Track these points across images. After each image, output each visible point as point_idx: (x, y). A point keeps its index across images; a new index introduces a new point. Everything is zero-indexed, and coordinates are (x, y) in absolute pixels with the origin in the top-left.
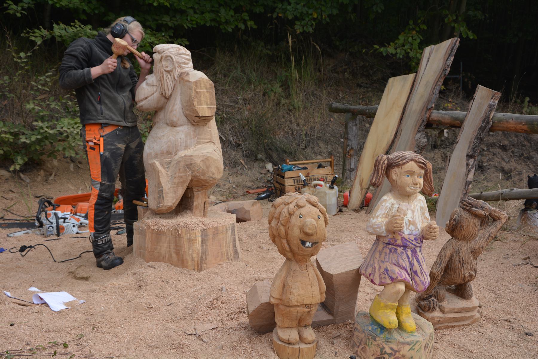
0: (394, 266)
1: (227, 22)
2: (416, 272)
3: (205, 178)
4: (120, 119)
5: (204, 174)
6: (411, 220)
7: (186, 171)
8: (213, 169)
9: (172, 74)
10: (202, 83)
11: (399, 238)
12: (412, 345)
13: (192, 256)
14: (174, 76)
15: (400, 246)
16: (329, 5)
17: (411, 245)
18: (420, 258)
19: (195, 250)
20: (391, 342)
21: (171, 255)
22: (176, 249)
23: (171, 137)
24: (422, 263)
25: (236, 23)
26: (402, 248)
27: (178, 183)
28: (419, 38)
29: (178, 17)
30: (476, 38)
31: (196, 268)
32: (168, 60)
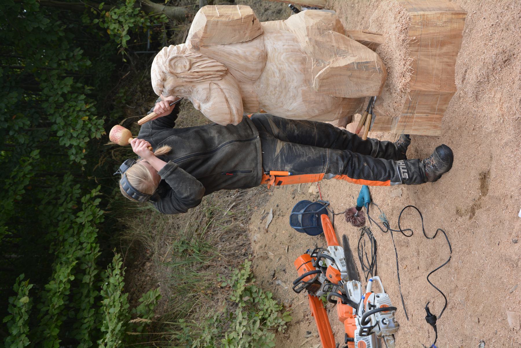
1: (94, 214)
4: (252, 147)
9: (194, 61)
13: (445, 22)
14: (197, 57)
16: (75, 104)
19: (438, 18)
21: (446, 54)
22: (437, 46)
23: (282, 57)
28: (113, 10)
29: (84, 266)
31: (461, 16)
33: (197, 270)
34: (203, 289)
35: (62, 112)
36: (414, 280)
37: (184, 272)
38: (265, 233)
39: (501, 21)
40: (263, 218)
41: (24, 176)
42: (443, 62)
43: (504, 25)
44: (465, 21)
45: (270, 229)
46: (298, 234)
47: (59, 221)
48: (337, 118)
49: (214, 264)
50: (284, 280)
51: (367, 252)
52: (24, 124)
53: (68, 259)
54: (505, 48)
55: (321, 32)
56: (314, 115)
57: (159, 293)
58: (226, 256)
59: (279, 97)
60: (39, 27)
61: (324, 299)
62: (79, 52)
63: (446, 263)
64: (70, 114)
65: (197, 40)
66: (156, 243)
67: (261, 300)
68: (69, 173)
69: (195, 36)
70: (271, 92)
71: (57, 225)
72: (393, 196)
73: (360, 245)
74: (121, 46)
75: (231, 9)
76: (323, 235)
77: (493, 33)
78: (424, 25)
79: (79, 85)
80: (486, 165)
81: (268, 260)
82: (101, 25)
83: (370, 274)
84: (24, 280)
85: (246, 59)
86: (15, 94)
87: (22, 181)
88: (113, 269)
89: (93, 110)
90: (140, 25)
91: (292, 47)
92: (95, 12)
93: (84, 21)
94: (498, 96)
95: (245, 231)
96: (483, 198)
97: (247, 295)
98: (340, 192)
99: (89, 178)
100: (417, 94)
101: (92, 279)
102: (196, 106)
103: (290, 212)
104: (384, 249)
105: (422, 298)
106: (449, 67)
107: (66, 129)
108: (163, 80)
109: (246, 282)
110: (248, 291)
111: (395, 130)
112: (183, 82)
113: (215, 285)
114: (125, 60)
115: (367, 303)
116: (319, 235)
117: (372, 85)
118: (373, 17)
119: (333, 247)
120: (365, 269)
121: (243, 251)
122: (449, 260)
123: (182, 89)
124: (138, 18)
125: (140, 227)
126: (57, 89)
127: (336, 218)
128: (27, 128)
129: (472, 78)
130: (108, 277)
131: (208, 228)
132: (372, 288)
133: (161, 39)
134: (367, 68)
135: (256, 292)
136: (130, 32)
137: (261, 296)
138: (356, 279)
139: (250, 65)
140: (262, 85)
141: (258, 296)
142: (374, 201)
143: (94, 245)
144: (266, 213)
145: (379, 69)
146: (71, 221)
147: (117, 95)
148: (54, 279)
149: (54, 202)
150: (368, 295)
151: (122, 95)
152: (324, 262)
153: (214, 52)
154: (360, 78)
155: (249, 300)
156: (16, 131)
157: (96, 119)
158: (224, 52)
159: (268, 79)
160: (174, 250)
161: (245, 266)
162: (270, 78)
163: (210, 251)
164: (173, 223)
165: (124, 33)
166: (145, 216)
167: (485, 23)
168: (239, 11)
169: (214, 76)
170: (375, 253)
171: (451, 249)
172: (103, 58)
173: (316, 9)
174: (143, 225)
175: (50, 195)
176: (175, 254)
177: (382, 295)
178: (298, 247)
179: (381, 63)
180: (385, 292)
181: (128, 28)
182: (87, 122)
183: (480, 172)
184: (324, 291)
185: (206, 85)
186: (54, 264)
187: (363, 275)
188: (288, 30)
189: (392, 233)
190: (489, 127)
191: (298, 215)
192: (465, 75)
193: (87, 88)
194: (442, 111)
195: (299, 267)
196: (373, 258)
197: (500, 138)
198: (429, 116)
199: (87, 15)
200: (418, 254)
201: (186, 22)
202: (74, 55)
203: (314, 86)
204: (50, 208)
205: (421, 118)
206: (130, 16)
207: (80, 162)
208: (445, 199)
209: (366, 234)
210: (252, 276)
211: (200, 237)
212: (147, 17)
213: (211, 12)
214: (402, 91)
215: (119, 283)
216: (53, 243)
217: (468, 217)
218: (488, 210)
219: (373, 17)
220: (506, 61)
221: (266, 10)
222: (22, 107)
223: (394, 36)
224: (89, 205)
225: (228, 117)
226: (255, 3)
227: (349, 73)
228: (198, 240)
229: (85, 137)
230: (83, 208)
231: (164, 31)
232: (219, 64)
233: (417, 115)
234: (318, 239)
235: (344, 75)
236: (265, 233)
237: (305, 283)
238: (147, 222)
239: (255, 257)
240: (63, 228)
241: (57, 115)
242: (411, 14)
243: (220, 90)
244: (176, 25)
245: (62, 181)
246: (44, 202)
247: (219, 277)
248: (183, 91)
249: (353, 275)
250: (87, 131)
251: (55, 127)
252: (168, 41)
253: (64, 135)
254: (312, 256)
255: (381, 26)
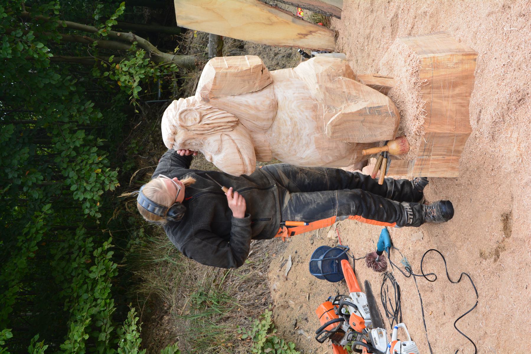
9: (204, 113)
13: (456, 63)
14: (207, 110)
16: (87, 157)
19: (449, 60)
21: (459, 95)
22: (449, 87)
25: (106, 261)
28: (123, 62)
29: (100, 323)
30: (124, 3)
31: (472, 57)
32: (185, 118)
33: (217, 322)
34: (224, 342)
35: (75, 165)
36: (441, 326)
37: (203, 325)
38: (284, 281)
39: (513, 61)
40: (282, 266)
41: (37, 232)
42: (456, 103)
43: (516, 65)
44: (476, 62)
45: (289, 277)
46: (319, 281)
47: (73, 277)
48: (352, 164)
49: (234, 315)
50: (306, 329)
51: (391, 298)
52: (37, 179)
53: (83, 316)
54: (518, 88)
55: (331, 78)
56: (328, 162)
57: (177, 348)
58: (245, 306)
59: (292, 145)
60: (50, 83)
61: (348, 348)
62: (90, 105)
63: (473, 309)
64: (83, 167)
65: (207, 92)
66: (173, 296)
67: (283, 352)
68: (81, 226)
69: (204, 88)
70: (283, 140)
71: (71, 282)
72: (414, 239)
73: (383, 290)
74: (133, 98)
75: (239, 60)
76: (345, 281)
77: (506, 73)
78: (435, 68)
79: (91, 137)
80: (508, 206)
81: (289, 309)
82: (112, 78)
83: (395, 321)
84: (39, 340)
85: (257, 109)
86: (26, 150)
87: (35, 237)
88: (130, 325)
89: (106, 161)
90: (150, 75)
91: (302, 94)
92: (105, 65)
93: (94, 74)
94: (515, 135)
95: (264, 280)
96: (506, 240)
97: (268, 347)
98: (359, 234)
99: (103, 231)
100: (431, 136)
101: (108, 337)
102: (208, 158)
103: (309, 259)
104: (408, 294)
105: (451, 346)
106: (463, 108)
107: (79, 183)
108: (174, 134)
109: (268, 333)
110: (269, 342)
111: (412, 173)
112: (194, 135)
113: (235, 337)
114: (137, 111)
115: (394, 352)
116: (341, 281)
117: (386, 129)
118: (383, 60)
119: (355, 293)
120: (390, 315)
121: (263, 300)
122: (476, 305)
123: (194, 142)
124: (148, 69)
125: (157, 280)
126: (69, 143)
127: (357, 263)
128: (40, 183)
129: (487, 118)
130: (124, 333)
131: (226, 278)
132: (398, 335)
133: (172, 88)
134: (380, 113)
135: (278, 343)
136: (140, 84)
137: (283, 347)
138: (381, 327)
139: (261, 115)
140: (274, 134)
141: (280, 348)
142: (395, 245)
143: (108, 301)
144: (284, 260)
145: (392, 113)
146: (85, 276)
147: (130, 146)
148: (69, 339)
149: (67, 257)
150: (394, 343)
151: (134, 145)
152: (346, 309)
153: (224, 104)
154: (373, 123)
155: (271, 352)
156: (29, 187)
157: (109, 171)
158: (234, 103)
159: (279, 128)
160: (192, 302)
161: (266, 316)
162: (281, 127)
163: (229, 301)
164: (190, 274)
165: (136, 84)
166: (161, 268)
167: (497, 63)
168: (248, 62)
169: (225, 127)
170: (399, 299)
171: (477, 293)
172: (114, 109)
173: (326, 52)
174: (159, 278)
175: (63, 249)
176: (193, 306)
177: (409, 343)
178: (319, 294)
179: (393, 107)
180: (412, 340)
181: (139, 80)
182: (100, 175)
183: (502, 213)
184: (348, 340)
185: (217, 137)
186: (69, 322)
187: (387, 322)
188: (298, 78)
189: (415, 277)
190: (507, 167)
191: (317, 261)
192: (480, 115)
193: (100, 141)
194: (459, 152)
195: (321, 316)
196: (397, 304)
197: (520, 179)
198: (446, 158)
199: (97, 68)
200: (444, 299)
201: (196, 70)
202: (85, 109)
203: (326, 132)
204: (63, 264)
205: (438, 160)
206: (140, 67)
207: (94, 215)
208: (468, 242)
209: (388, 279)
210: (273, 326)
211: (218, 288)
212: (157, 67)
213: (219, 64)
214: (416, 134)
215: (136, 340)
216: (67, 300)
217: (492, 260)
218: (513, 252)
219: (383, 60)
220: (520, 100)
221: (276, 54)
222: (35, 161)
223: (405, 80)
224: (102, 259)
225: (241, 168)
226: (264, 48)
227: (362, 118)
228: (216, 291)
229: (99, 190)
230: (96, 263)
231: (175, 80)
232: (229, 115)
233: (433, 157)
234: (339, 285)
235: (357, 121)
236: (284, 281)
237: (329, 332)
238: (163, 274)
239: (275, 306)
240: (77, 285)
241: (70, 169)
242: (421, 57)
243: (231, 141)
244: (186, 73)
245: (75, 234)
246: (57, 258)
247: (239, 329)
248: (194, 144)
249: (378, 323)
250: (101, 184)
251: (68, 181)
252: (178, 89)
253: (77, 190)
254: (334, 304)
255: (391, 69)
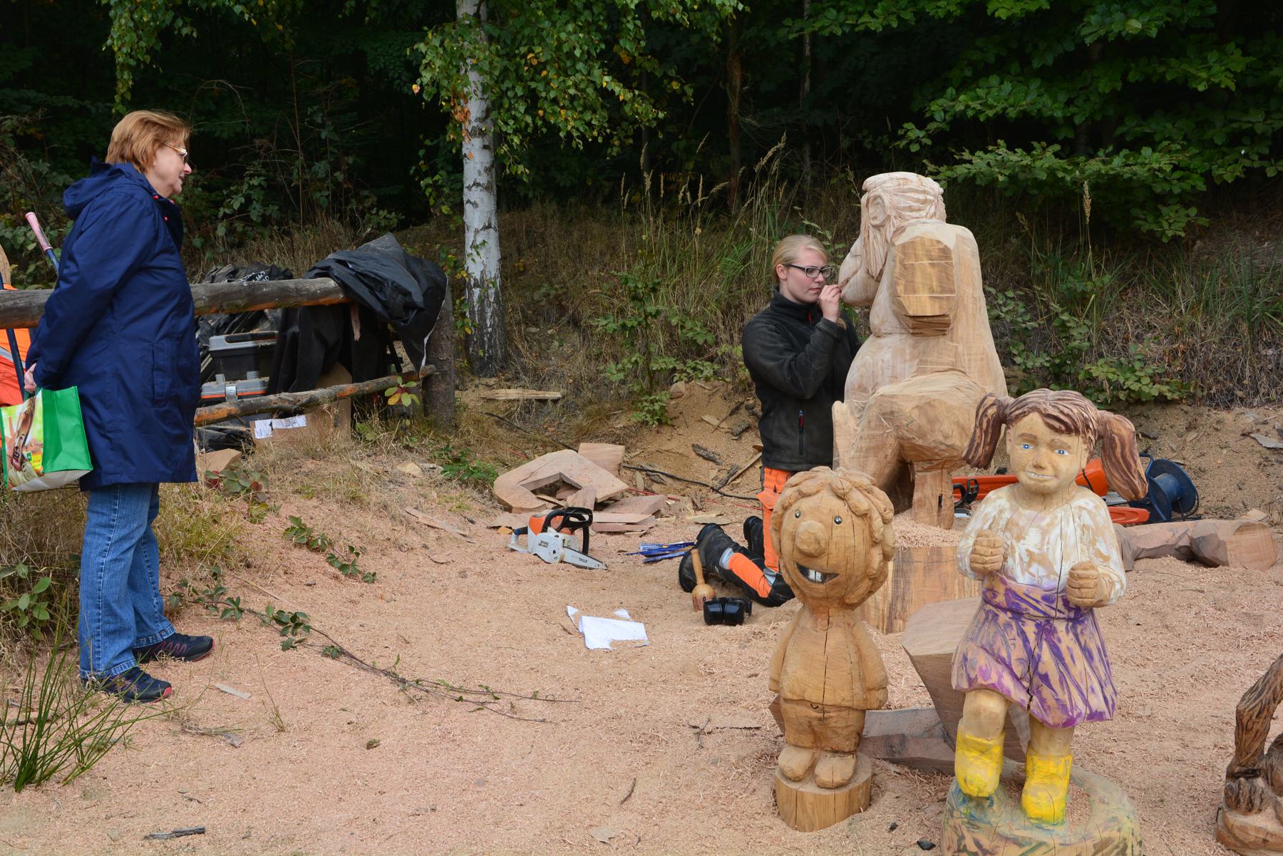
0: (982, 651)
2: (1045, 678)
3: (926, 444)
5: (923, 436)
6: (1035, 551)
7: (881, 425)
8: (946, 427)
10: (919, 247)
11: (1001, 589)
12: (1027, 848)
15: (1005, 610)
17: (1032, 611)
18: (1063, 647)
20: (978, 828)
24: (1068, 660)
26: (1009, 614)
27: (868, 449)
